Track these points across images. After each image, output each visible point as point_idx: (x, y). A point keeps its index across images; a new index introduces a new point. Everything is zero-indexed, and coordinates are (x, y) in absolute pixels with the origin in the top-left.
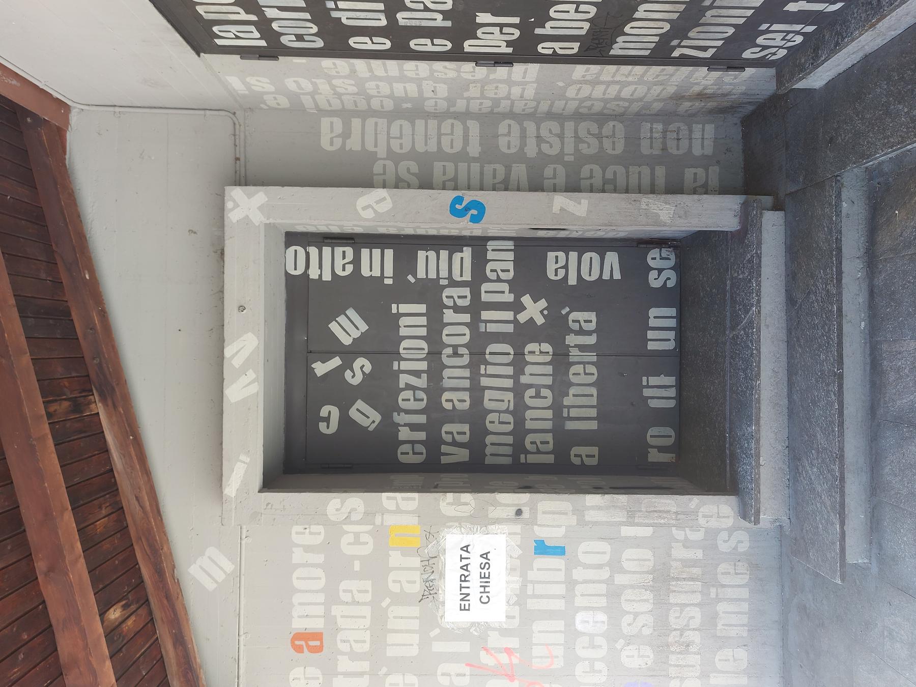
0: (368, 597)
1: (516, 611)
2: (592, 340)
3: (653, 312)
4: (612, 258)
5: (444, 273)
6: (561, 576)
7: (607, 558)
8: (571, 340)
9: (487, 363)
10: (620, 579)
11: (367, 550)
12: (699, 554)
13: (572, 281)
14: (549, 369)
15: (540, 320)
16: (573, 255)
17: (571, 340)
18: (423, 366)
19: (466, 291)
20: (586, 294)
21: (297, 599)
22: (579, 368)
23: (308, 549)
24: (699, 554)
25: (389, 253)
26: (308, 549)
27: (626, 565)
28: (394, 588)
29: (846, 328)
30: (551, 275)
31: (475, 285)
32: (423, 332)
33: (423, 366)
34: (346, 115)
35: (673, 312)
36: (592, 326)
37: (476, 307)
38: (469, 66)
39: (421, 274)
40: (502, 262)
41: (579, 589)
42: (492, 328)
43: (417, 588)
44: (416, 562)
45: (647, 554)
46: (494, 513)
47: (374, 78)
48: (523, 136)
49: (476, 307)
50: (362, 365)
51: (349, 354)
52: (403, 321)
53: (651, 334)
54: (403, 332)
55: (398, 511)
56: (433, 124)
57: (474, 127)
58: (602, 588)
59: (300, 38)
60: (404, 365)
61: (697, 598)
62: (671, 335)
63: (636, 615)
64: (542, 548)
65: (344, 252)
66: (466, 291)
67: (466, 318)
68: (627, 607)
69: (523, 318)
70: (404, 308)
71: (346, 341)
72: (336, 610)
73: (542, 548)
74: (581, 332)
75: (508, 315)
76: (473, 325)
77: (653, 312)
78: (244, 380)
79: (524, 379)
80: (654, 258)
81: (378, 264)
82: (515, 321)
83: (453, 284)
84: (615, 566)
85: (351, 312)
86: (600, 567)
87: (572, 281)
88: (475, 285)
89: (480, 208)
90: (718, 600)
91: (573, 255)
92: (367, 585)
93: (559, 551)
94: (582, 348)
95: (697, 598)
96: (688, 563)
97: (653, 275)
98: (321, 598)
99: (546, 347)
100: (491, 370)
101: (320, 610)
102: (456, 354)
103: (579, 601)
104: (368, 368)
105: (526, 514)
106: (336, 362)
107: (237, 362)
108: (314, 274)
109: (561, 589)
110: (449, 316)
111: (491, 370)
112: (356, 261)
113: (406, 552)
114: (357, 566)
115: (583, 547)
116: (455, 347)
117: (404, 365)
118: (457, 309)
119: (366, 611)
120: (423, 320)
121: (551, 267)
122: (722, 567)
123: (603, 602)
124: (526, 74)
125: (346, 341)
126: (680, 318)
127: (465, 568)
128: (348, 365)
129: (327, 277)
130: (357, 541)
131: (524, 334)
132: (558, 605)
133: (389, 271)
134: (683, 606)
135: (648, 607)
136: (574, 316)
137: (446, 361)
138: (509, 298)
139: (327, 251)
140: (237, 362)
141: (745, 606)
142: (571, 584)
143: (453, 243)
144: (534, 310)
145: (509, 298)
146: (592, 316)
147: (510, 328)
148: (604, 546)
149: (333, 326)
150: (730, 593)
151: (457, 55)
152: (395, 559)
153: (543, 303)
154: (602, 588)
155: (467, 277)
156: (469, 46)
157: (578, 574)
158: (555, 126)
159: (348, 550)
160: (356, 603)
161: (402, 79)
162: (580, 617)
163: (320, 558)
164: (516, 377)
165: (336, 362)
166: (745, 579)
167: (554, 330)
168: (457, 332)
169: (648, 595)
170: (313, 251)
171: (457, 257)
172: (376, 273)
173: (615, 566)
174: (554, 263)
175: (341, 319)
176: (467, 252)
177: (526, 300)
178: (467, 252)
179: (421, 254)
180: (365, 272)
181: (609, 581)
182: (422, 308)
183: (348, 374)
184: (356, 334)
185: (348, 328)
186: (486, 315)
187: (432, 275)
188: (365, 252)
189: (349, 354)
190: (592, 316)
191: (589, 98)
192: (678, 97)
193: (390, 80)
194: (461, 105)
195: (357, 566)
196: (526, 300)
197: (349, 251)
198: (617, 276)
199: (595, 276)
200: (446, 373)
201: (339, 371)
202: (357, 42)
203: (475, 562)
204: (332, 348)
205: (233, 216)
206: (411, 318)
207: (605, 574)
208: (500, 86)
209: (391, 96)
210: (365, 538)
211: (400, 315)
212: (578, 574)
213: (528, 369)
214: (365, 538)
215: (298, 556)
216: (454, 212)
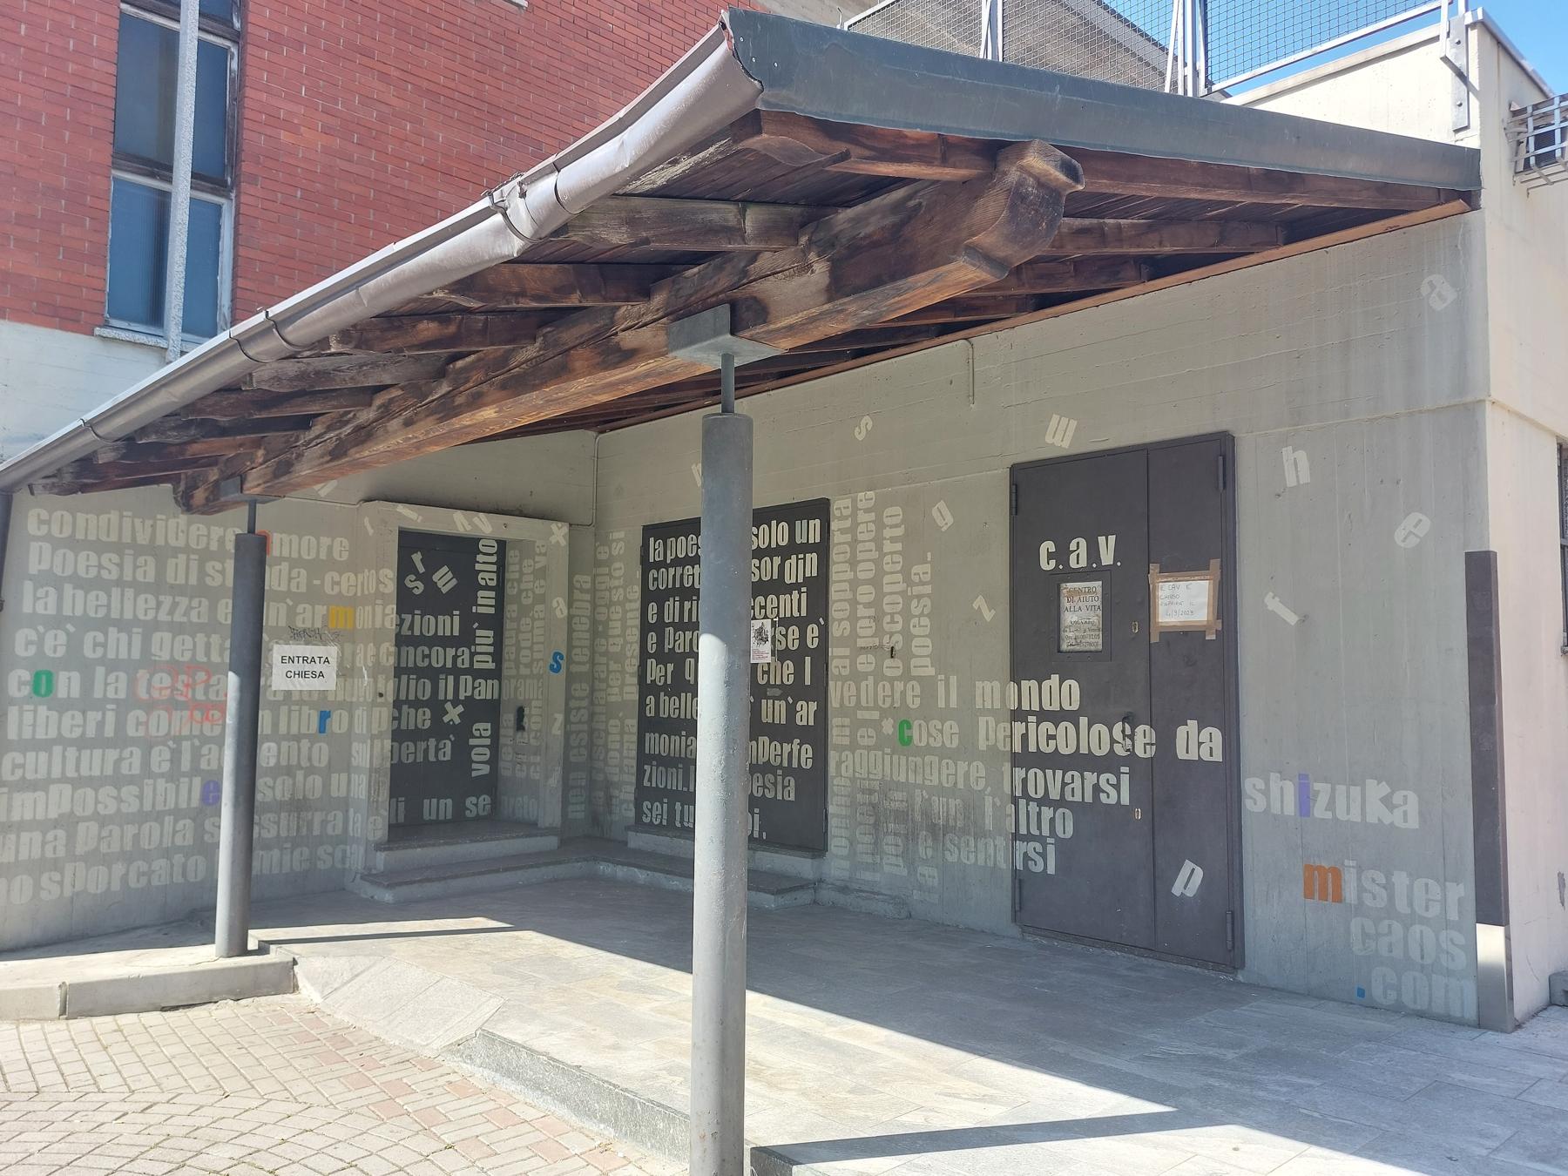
0: (294, 589)
1: (280, 697)
2: (432, 758)
3: (449, 801)
4: (485, 769)
5: (479, 649)
6: (304, 730)
7: (316, 764)
8: (432, 742)
9: (417, 680)
10: (300, 775)
11: (328, 589)
12: (316, 832)
13: (472, 742)
14: (412, 727)
15: (446, 719)
16: (488, 742)
17: (432, 742)
18: (417, 633)
19: (467, 665)
20: (463, 751)
21: (295, 538)
22: (412, 749)
23: (330, 548)
24: (316, 832)
25: (492, 611)
26: (330, 548)
27: (310, 779)
28: (300, 609)
29: (519, 873)
30: (476, 726)
31: (471, 671)
32: (440, 633)
33: (417, 633)
34: (594, 590)
35: (449, 817)
36: (441, 758)
37: (457, 672)
38: (636, 662)
39: (479, 632)
40: (485, 690)
41: (294, 745)
42: (442, 683)
43: (300, 625)
44: (318, 625)
45: (317, 795)
46: (381, 678)
47: (625, 612)
48: (581, 699)
49: (457, 672)
50: (419, 588)
51: (426, 579)
52: (448, 619)
53: (434, 801)
54: (441, 618)
55: (384, 615)
56: (587, 643)
57: (585, 668)
58: (294, 762)
59: (655, 579)
60: (417, 618)
61: (284, 834)
62: (434, 817)
63: (273, 788)
64: (324, 716)
65: (1405, 821)
66: (467, 665)
67: (449, 665)
68: (279, 781)
69: (448, 706)
70: (456, 619)
71: (435, 578)
72: (285, 566)
73: (324, 716)
74: (437, 750)
75: (450, 696)
76: (443, 670)
77: (449, 801)
78: (466, 523)
79: (405, 707)
80: (485, 800)
81: (485, 602)
82: (446, 701)
83: (472, 655)
84: (311, 770)
85: (454, 582)
86: (310, 759)
87: (472, 742)
88: (471, 671)
89: (557, 671)
90: (282, 849)
91: (488, 742)
92: (303, 589)
93: (322, 728)
94: (426, 751)
95: (284, 834)
96: (310, 824)
97: (474, 799)
98: (294, 555)
99: (428, 724)
100: (413, 683)
101: (285, 553)
102: (424, 656)
103: (285, 745)
104: (417, 592)
105: (380, 700)
106: (421, 569)
107: (476, 520)
108: (480, 558)
109: (294, 730)
110: (451, 652)
111: (413, 683)
112: (487, 588)
113: (325, 618)
114: (317, 582)
115: (325, 746)
116: (429, 656)
117: (417, 618)
118: (455, 658)
119: (283, 588)
120: (448, 633)
121: (481, 726)
122: (306, 851)
123: (284, 763)
124: (632, 693)
125: (435, 578)
126: (446, 822)
127: (313, 660)
128: (419, 577)
129: (478, 567)
130: (334, 583)
131: (437, 706)
132: (283, 729)
133: (481, 610)
134: (278, 823)
135: (279, 796)
136: (449, 743)
137: (420, 649)
138: (462, 697)
139: (494, 568)
140: (476, 520)
141: (276, 871)
142: (297, 738)
143: (498, 656)
144: (453, 714)
145: (462, 697)
146: (448, 757)
147: (441, 697)
148: (324, 763)
149: (445, 569)
150: (287, 858)
151: (644, 655)
152: (321, 610)
153: (457, 721)
154: (294, 762)
155: (476, 666)
156: (651, 662)
157: (305, 743)
158: (585, 718)
159: (328, 578)
160: (290, 579)
161: (624, 627)
162: (273, 745)
163: (323, 556)
164: (407, 701)
165: (421, 569)
166: (297, 867)
167: (439, 729)
168: (441, 657)
169: (287, 796)
170: (494, 559)
171: (489, 658)
172: (480, 601)
173: (311, 770)
174: (483, 728)
175: (450, 575)
176: (491, 666)
177: (460, 709)
178: (491, 666)
179: (490, 633)
180: (481, 593)
181: (299, 767)
182: (456, 633)
183: (413, 577)
184: (440, 584)
185: (444, 579)
186: (451, 678)
187: (478, 641)
188: (492, 594)
189: (426, 579)
190: (448, 757)
191: (608, 733)
192: (608, 785)
193: (623, 620)
194: (599, 659)
195: (317, 582)
196: (460, 709)
197: (493, 583)
198: (474, 774)
199: (475, 758)
200: (411, 650)
201: (416, 572)
202: (653, 608)
203: (317, 668)
204: (432, 567)
205: (554, 526)
206: (450, 625)
207: (304, 763)
208: (769, 644)
209: (609, 619)
210: (337, 589)
211: (452, 616)
212: (305, 743)
213: (412, 711)
214: (337, 589)
215: (325, 541)
216: (556, 654)
